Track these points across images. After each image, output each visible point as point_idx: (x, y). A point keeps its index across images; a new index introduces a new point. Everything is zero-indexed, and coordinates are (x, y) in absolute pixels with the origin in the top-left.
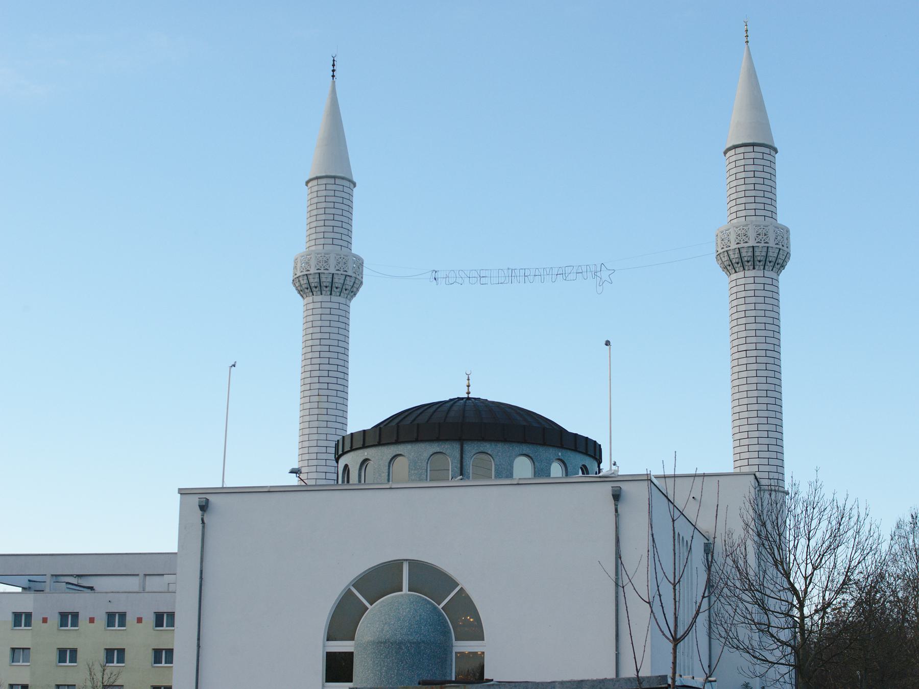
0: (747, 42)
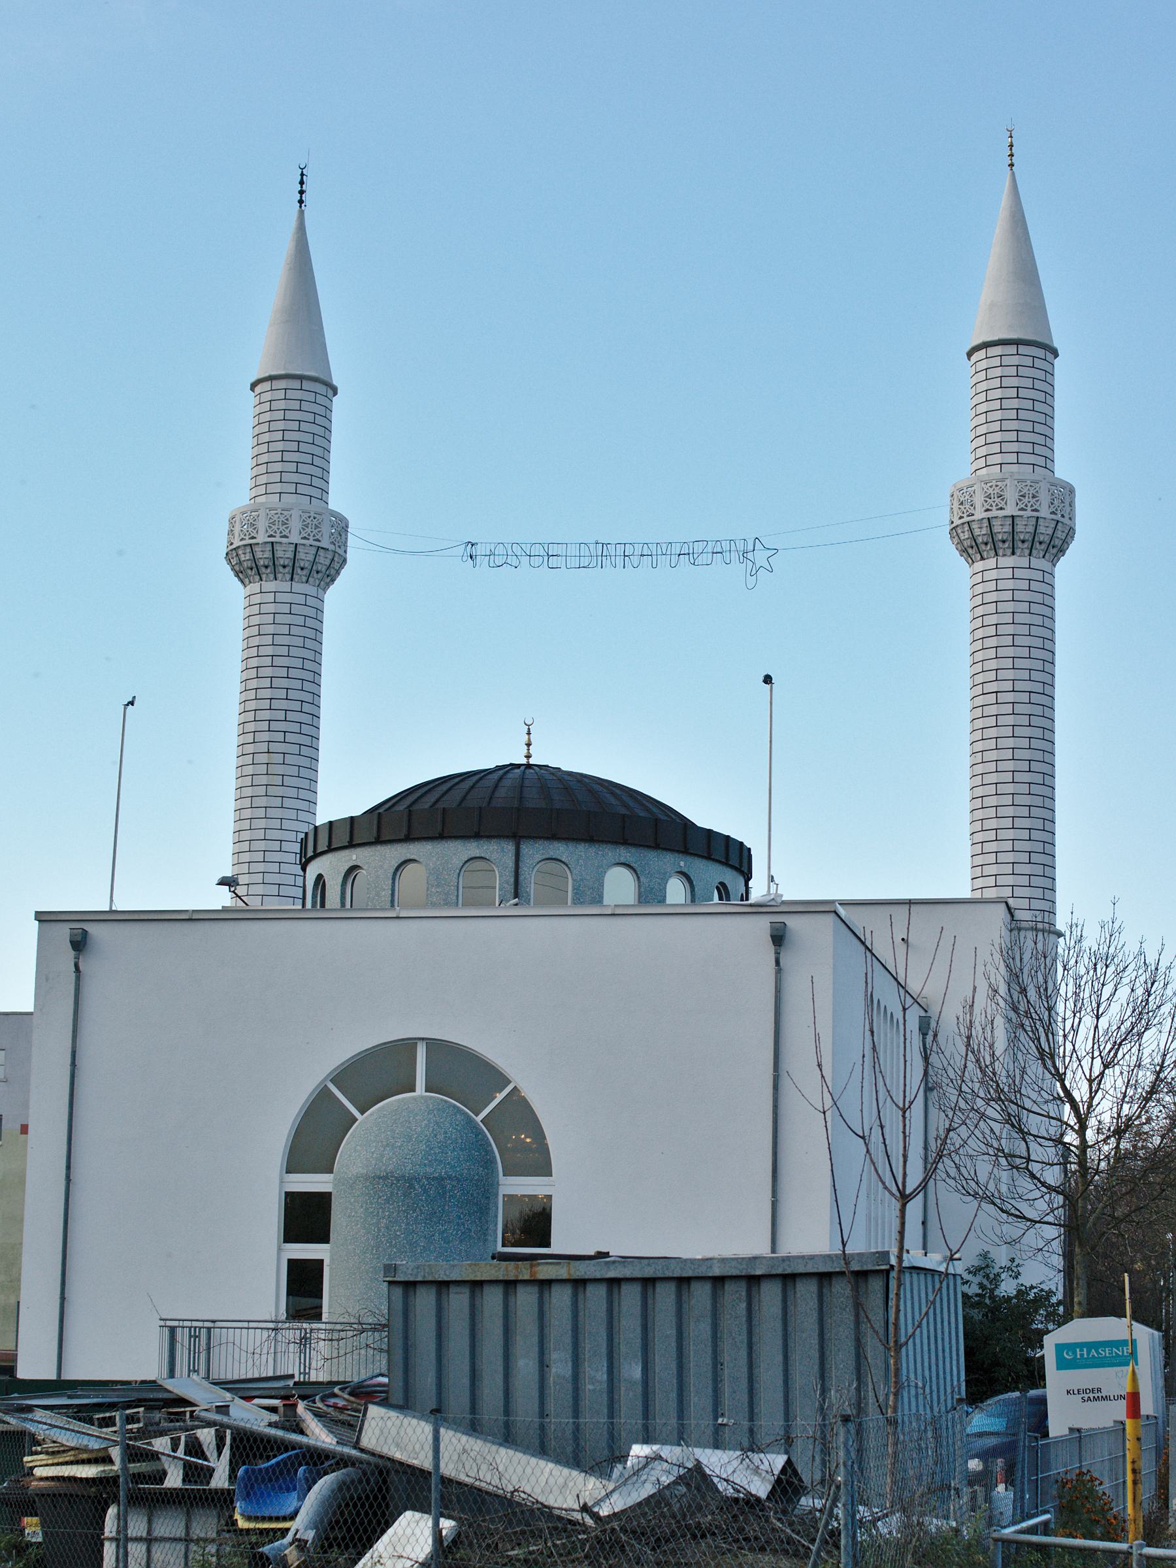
0: (1012, 165)
